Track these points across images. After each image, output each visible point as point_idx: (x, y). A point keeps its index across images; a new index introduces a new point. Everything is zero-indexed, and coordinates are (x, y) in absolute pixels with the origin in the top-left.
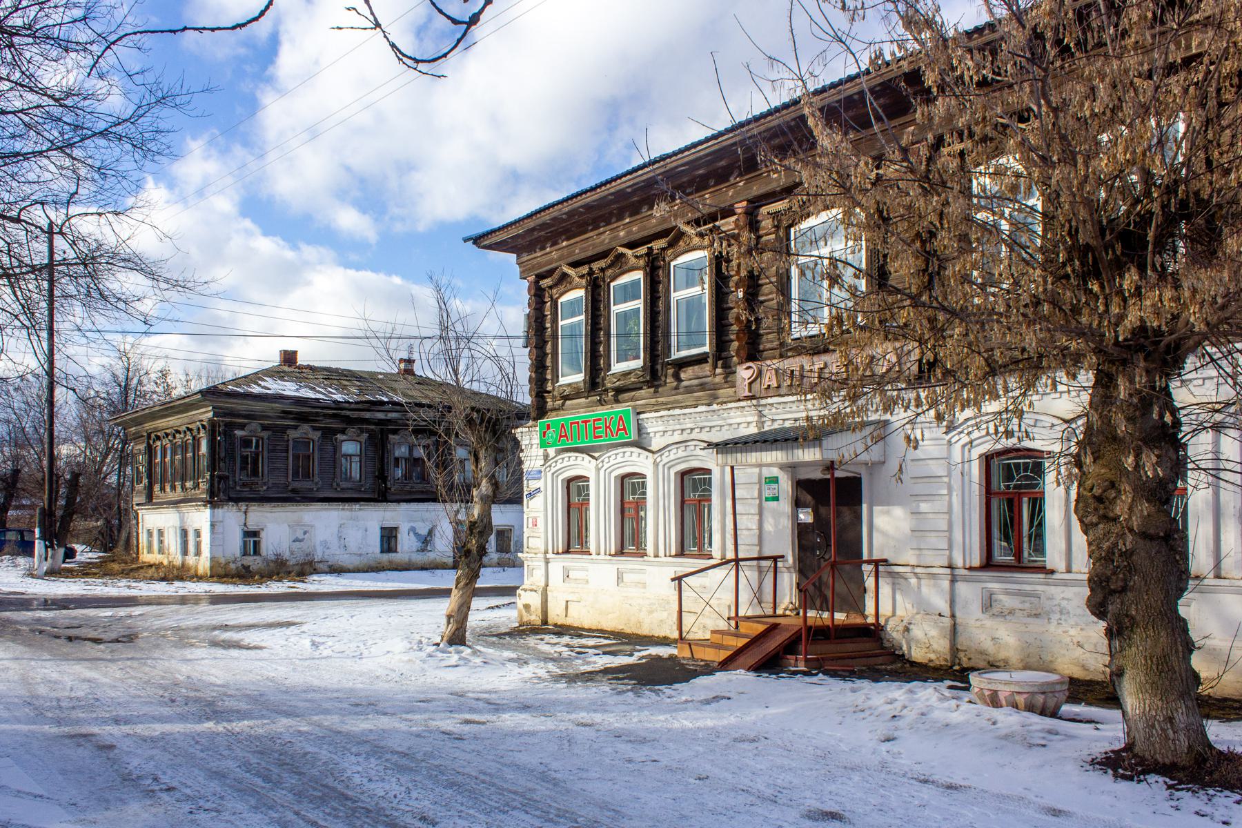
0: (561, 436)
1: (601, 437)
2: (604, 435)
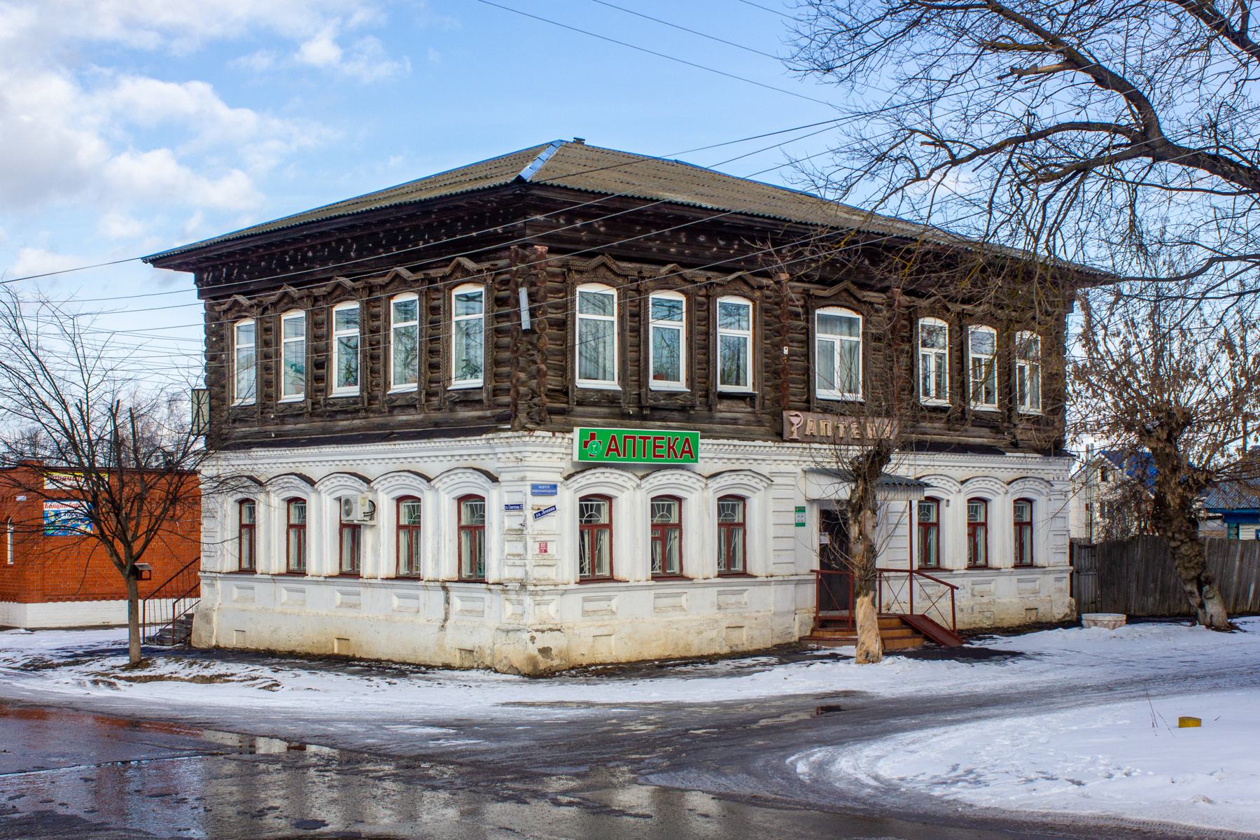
0: (610, 449)
1: (663, 456)
2: (666, 455)
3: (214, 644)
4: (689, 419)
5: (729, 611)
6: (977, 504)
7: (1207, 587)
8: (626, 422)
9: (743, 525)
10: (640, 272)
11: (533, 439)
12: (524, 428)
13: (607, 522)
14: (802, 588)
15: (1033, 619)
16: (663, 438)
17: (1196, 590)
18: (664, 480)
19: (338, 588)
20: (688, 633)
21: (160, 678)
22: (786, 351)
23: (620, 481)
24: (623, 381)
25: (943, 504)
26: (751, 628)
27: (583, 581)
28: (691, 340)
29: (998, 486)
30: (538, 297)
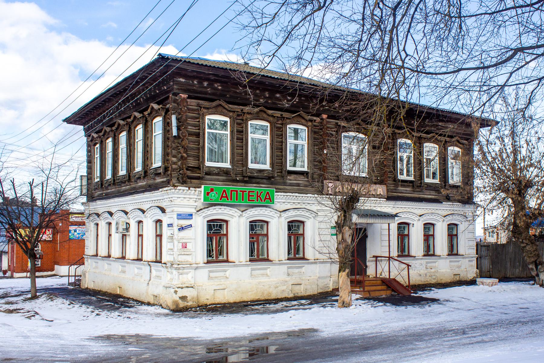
0: (222, 197)
1: (254, 201)
3: (86, 287)
4: (272, 184)
5: (294, 276)
6: (428, 227)
7: (540, 266)
8: (235, 184)
9: (303, 235)
10: (242, 110)
11: (177, 191)
12: (174, 186)
13: (302, 233)
14: (334, 265)
15: (458, 279)
16: (254, 192)
17: (534, 268)
18: (220, 211)
19: (120, 263)
20: (270, 287)
22: (325, 152)
23: (231, 213)
24: (232, 163)
25: (411, 226)
26: (305, 284)
27: (208, 262)
28: (272, 145)
29: (439, 218)
30: (182, 120)
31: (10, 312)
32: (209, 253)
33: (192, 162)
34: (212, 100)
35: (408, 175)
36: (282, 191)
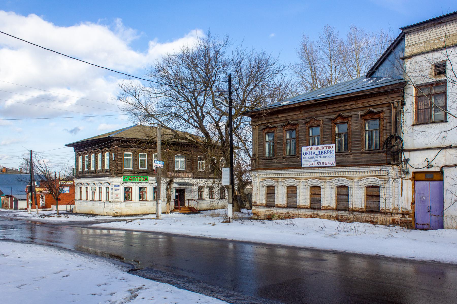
0: (130, 179)
12: (113, 176)
21: (52, 217)
23: (133, 184)
27: (125, 201)
31: (59, 217)
32: (125, 198)
33: (119, 168)
34: (127, 147)
35: (202, 169)
36: (392, 48)
